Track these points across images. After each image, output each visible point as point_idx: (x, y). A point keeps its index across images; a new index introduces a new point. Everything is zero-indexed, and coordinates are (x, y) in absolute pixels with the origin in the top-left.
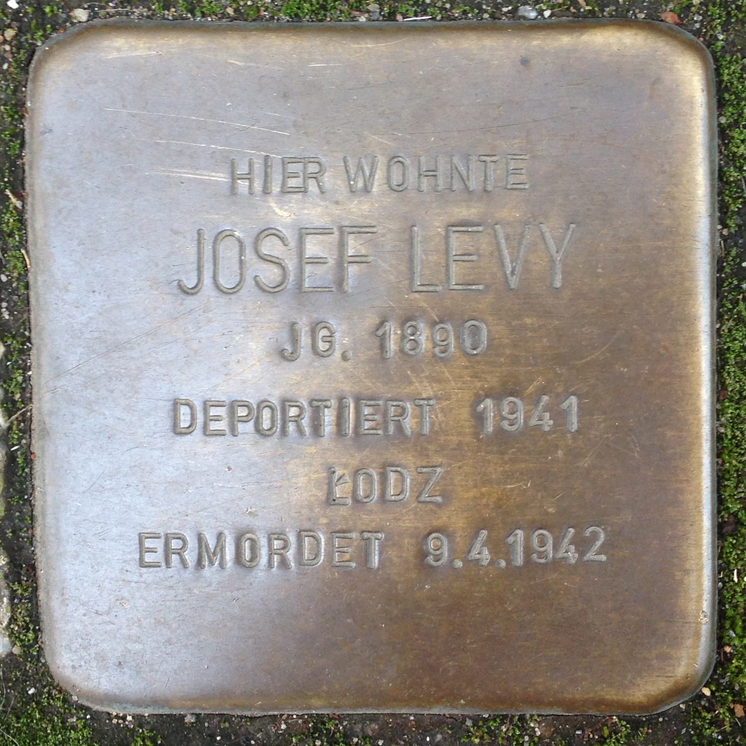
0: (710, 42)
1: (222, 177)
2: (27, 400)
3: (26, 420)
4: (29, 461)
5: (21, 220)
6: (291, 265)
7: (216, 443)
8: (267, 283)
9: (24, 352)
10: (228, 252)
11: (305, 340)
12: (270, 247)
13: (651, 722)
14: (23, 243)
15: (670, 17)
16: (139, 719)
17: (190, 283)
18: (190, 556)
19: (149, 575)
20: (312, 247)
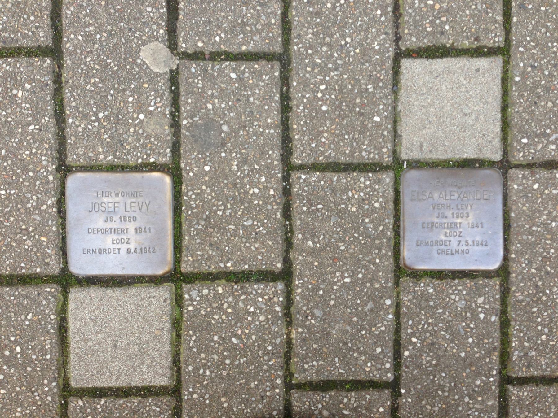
0: (173, 174)
1: (96, 194)
2: (65, 228)
3: (65, 231)
4: (66, 237)
5: (64, 200)
6: (107, 207)
7: (95, 235)
8: (406, 257)
9: (65, 221)
10: (97, 206)
11: (109, 219)
12: (103, 205)
13: (164, 277)
14: (65, 204)
15: (166, 170)
16: (83, 278)
17: (91, 210)
18: (91, 252)
19: (84, 255)
20: (110, 205)
